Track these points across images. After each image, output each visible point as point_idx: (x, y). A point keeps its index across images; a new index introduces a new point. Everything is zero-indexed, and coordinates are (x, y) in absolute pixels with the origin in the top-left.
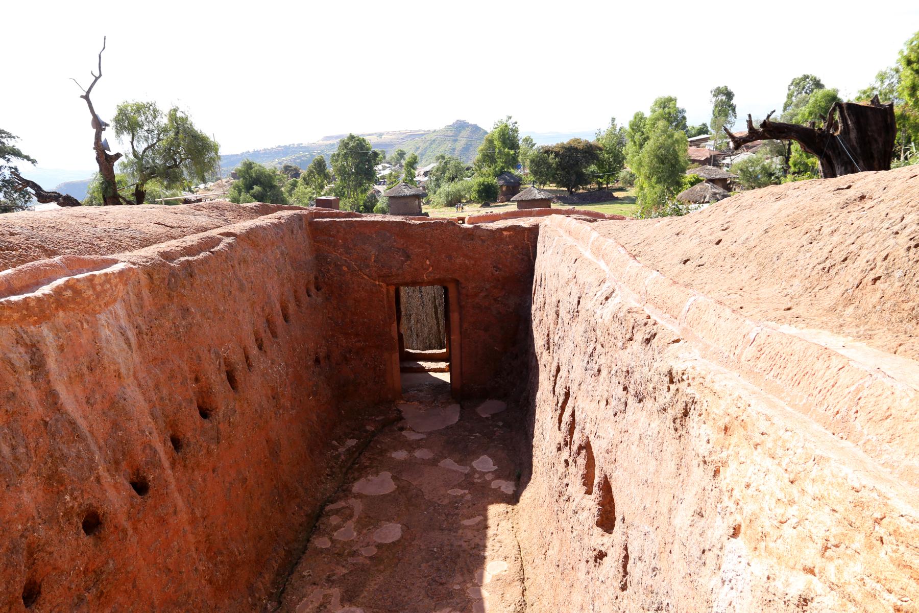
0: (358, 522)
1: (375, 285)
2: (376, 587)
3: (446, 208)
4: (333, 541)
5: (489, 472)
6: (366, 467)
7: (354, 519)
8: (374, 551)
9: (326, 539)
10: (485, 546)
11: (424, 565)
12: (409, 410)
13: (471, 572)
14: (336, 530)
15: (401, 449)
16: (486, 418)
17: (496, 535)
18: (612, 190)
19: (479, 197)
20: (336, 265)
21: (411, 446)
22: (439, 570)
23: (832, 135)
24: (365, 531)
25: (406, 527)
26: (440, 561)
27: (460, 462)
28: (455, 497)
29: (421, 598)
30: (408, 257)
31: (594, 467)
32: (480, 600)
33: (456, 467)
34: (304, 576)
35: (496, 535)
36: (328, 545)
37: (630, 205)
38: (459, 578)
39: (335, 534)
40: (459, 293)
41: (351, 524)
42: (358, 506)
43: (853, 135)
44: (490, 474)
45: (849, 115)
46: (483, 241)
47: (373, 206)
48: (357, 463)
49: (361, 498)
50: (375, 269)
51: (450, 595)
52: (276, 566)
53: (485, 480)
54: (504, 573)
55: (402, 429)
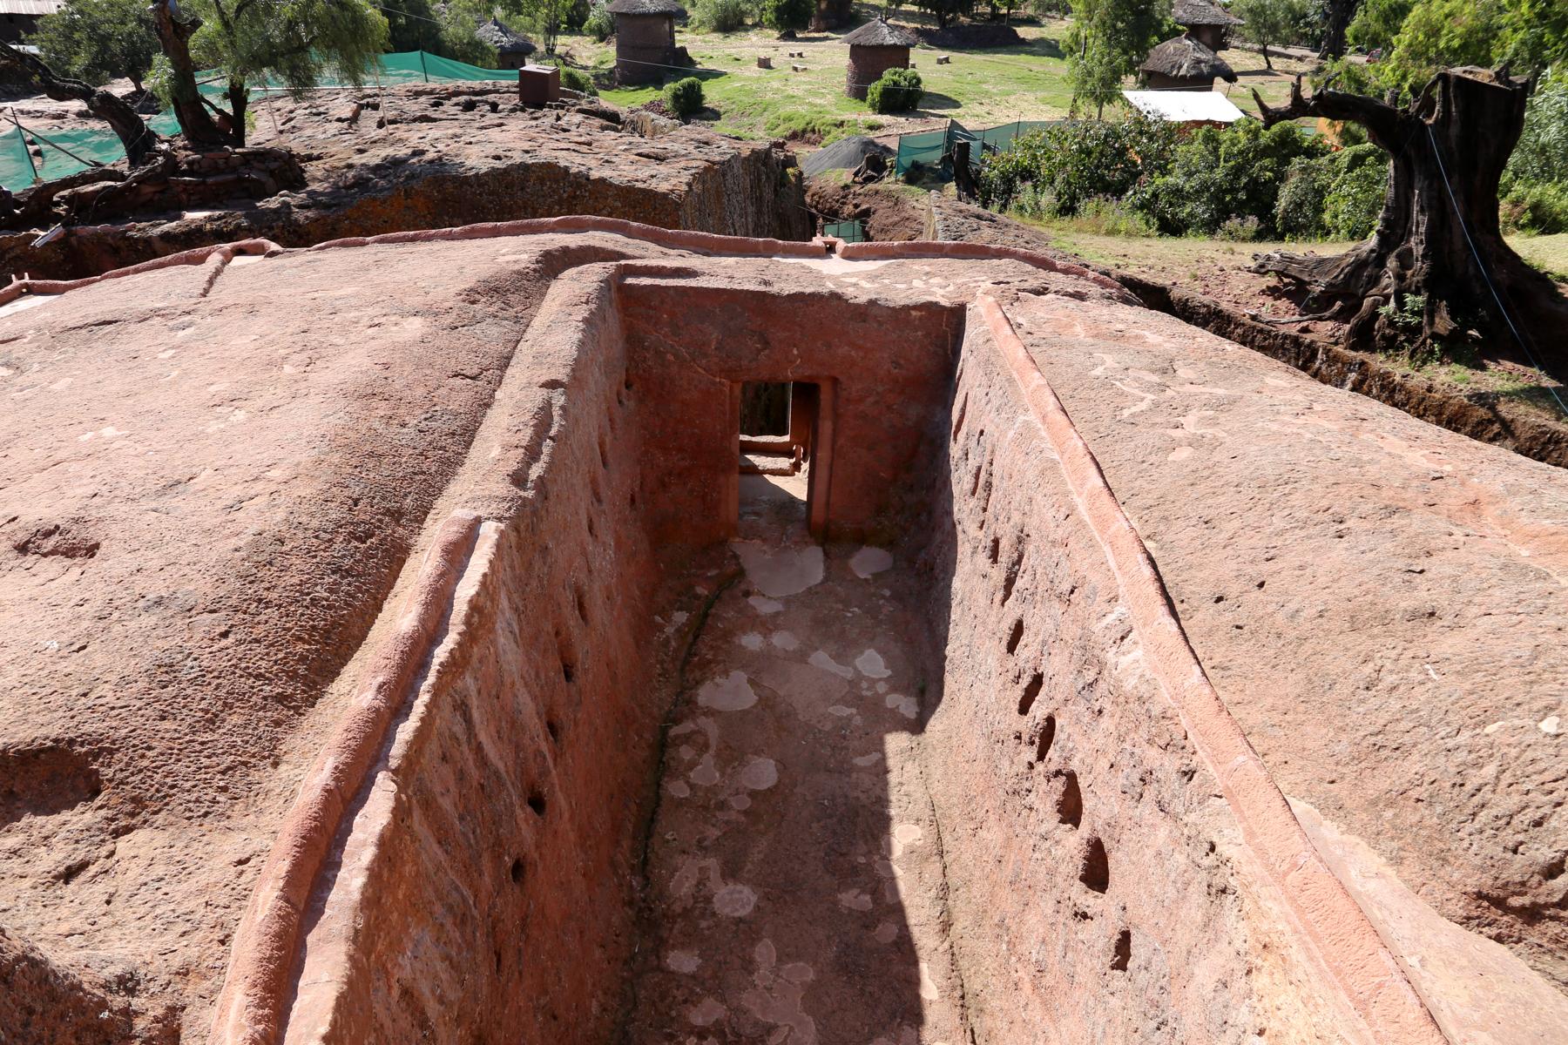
0: (718, 755)
1: (714, 383)
2: (761, 856)
3: (715, 35)
4: (692, 787)
5: (880, 679)
6: (710, 662)
7: (712, 751)
8: (748, 803)
9: (681, 783)
10: (888, 801)
11: (814, 825)
12: (753, 555)
13: (876, 838)
14: (691, 769)
15: (752, 631)
16: (866, 580)
17: (901, 784)
18: (1014, 20)
19: (777, 19)
20: (657, 352)
21: (767, 626)
22: (834, 833)
23: (1422, 123)
24: (729, 771)
25: (783, 766)
26: (835, 820)
27: (839, 658)
28: (840, 718)
29: (819, 873)
30: (766, 344)
31: (1027, 690)
32: (893, 878)
33: (833, 667)
34: (668, 841)
35: (901, 784)
36: (687, 793)
37: (1046, 58)
38: (863, 848)
39: (692, 775)
40: (836, 395)
41: (708, 759)
42: (712, 728)
43: (1454, 131)
44: (882, 683)
45: (1455, 97)
46: (880, 324)
47: (584, 19)
48: (696, 655)
49: (713, 715)
50: (716, 360)
51: (855, 870)
52: (630, 827)
53: (877, 693)
54: (918, 843)
55: (747, 594)
